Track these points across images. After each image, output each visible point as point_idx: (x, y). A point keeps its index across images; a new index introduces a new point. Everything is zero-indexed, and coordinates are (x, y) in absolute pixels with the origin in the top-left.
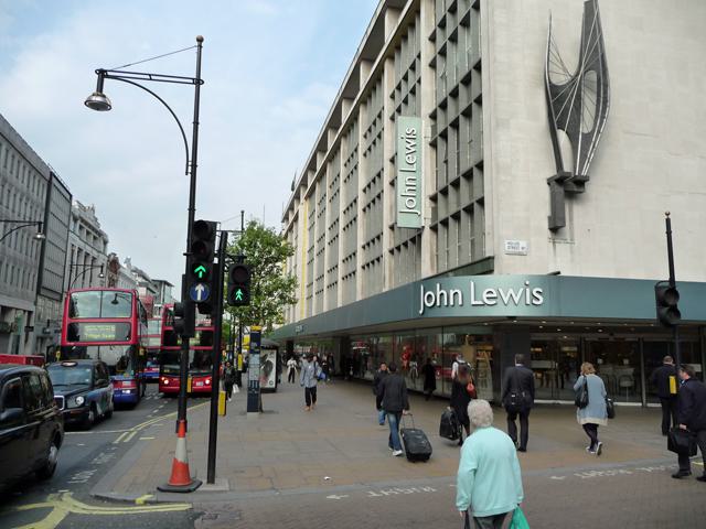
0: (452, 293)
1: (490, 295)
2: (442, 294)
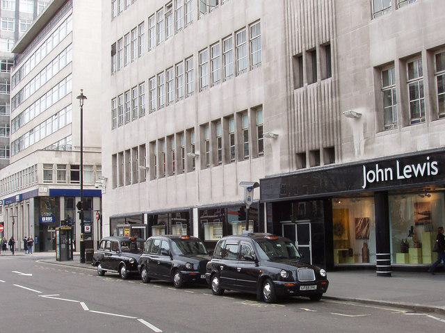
1: (408, 171)
2: (380, 173)
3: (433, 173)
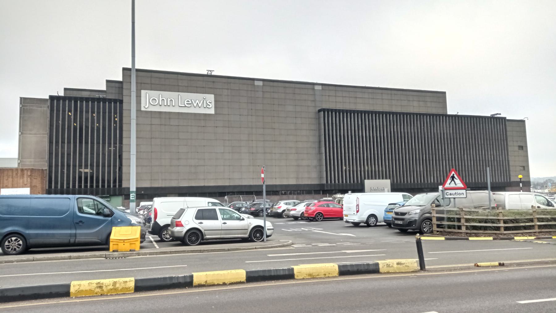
0: (169, 100)
1: (188, 103)
3: (208, 107)
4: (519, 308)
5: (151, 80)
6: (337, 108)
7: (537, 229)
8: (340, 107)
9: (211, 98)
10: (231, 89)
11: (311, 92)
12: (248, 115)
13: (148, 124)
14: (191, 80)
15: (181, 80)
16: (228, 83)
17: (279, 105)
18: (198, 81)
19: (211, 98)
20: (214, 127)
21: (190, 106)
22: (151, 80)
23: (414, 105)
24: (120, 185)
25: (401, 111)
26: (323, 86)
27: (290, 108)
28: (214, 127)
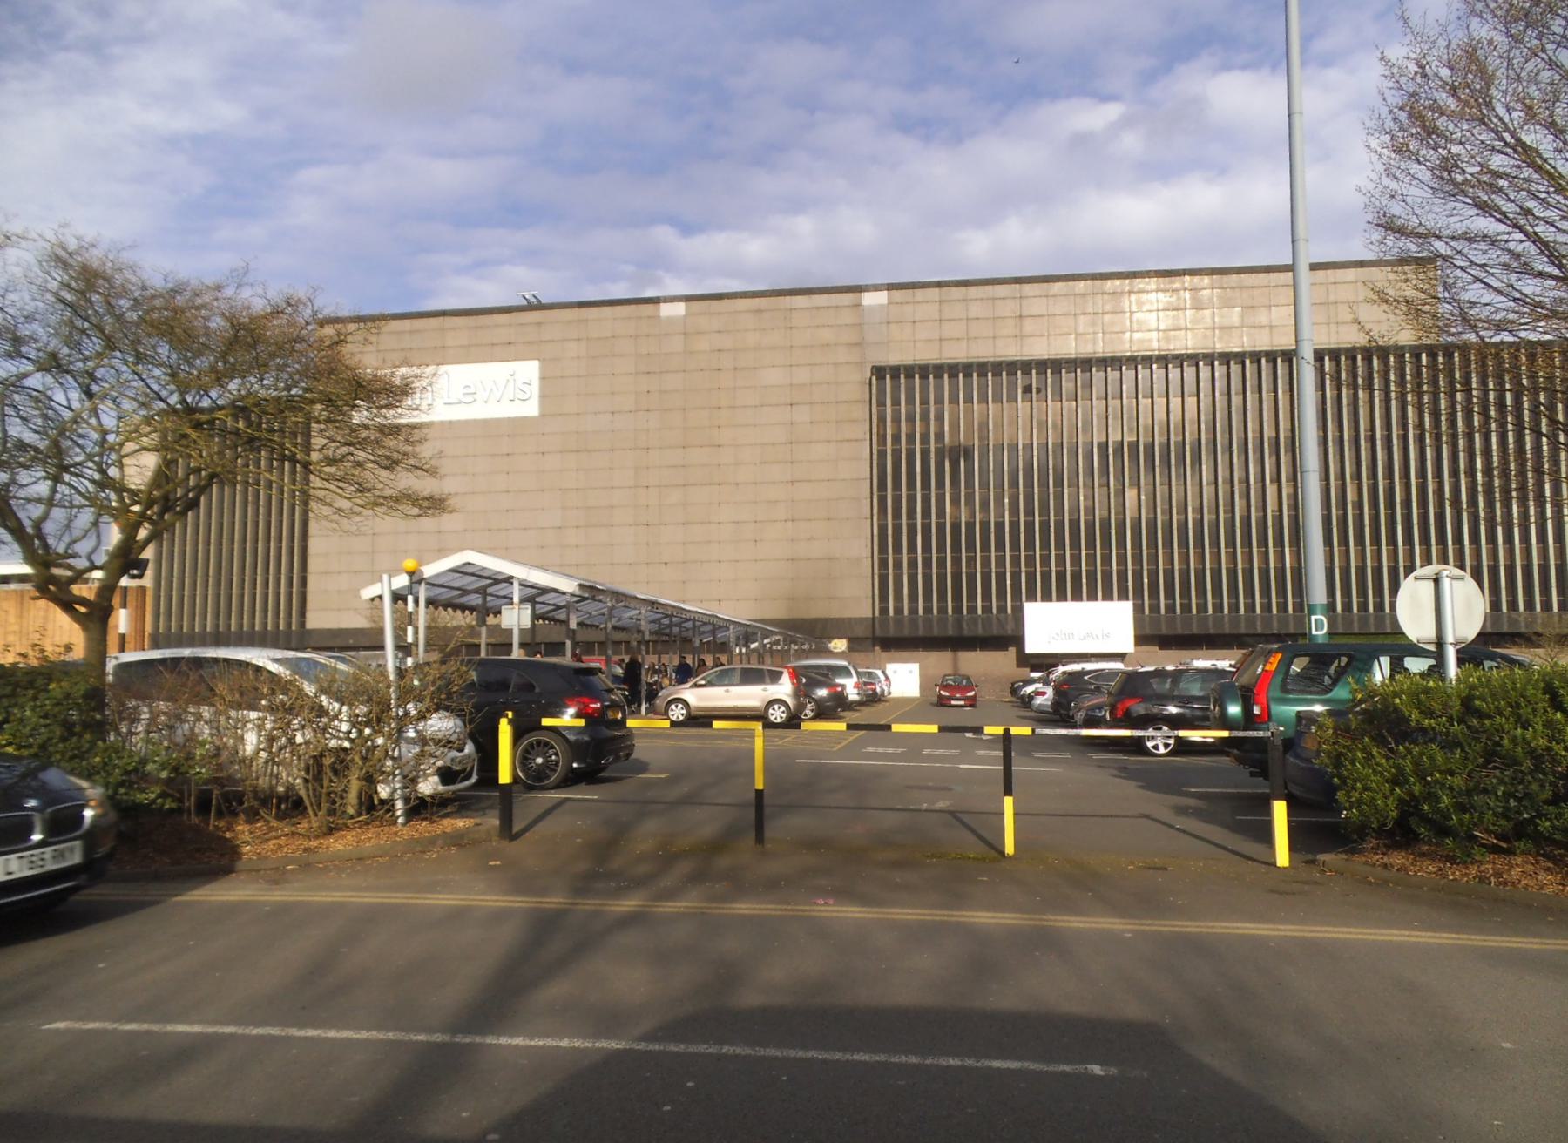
1: (466, 391)
4: (111, 438)
5: (210, 397)
6: (943, 361)
7: (1278, 688)
8: (957, 353)
9: (529, 370)
10: (588, 339)
11: (848, 317)
12: (636, 411)
13: (677, 486)
14: (476, 327)
15: (454, 329)
16: (580, 321)
17: (736, 369)
18: (497, 326)
19: (529, 370)
20: (537, 453)
21: (471, 400)
22: (210, 397)
23: (1273, 324)
24: (302, 624)
25: (1329, 344)
26: (894, 292)
27: (773, 376)
28: (537, 453)
